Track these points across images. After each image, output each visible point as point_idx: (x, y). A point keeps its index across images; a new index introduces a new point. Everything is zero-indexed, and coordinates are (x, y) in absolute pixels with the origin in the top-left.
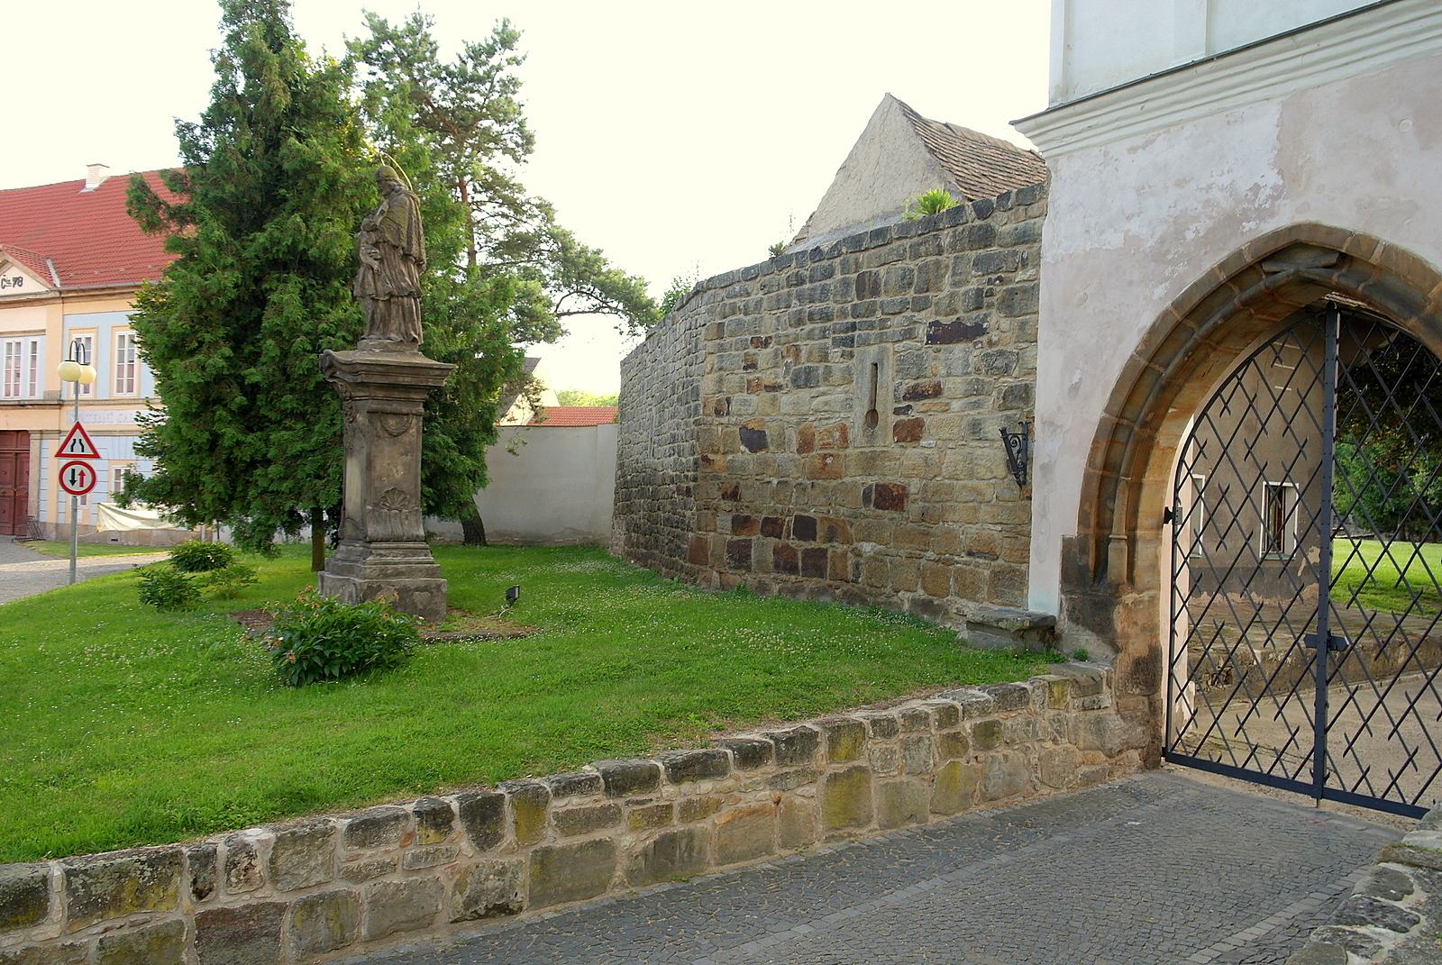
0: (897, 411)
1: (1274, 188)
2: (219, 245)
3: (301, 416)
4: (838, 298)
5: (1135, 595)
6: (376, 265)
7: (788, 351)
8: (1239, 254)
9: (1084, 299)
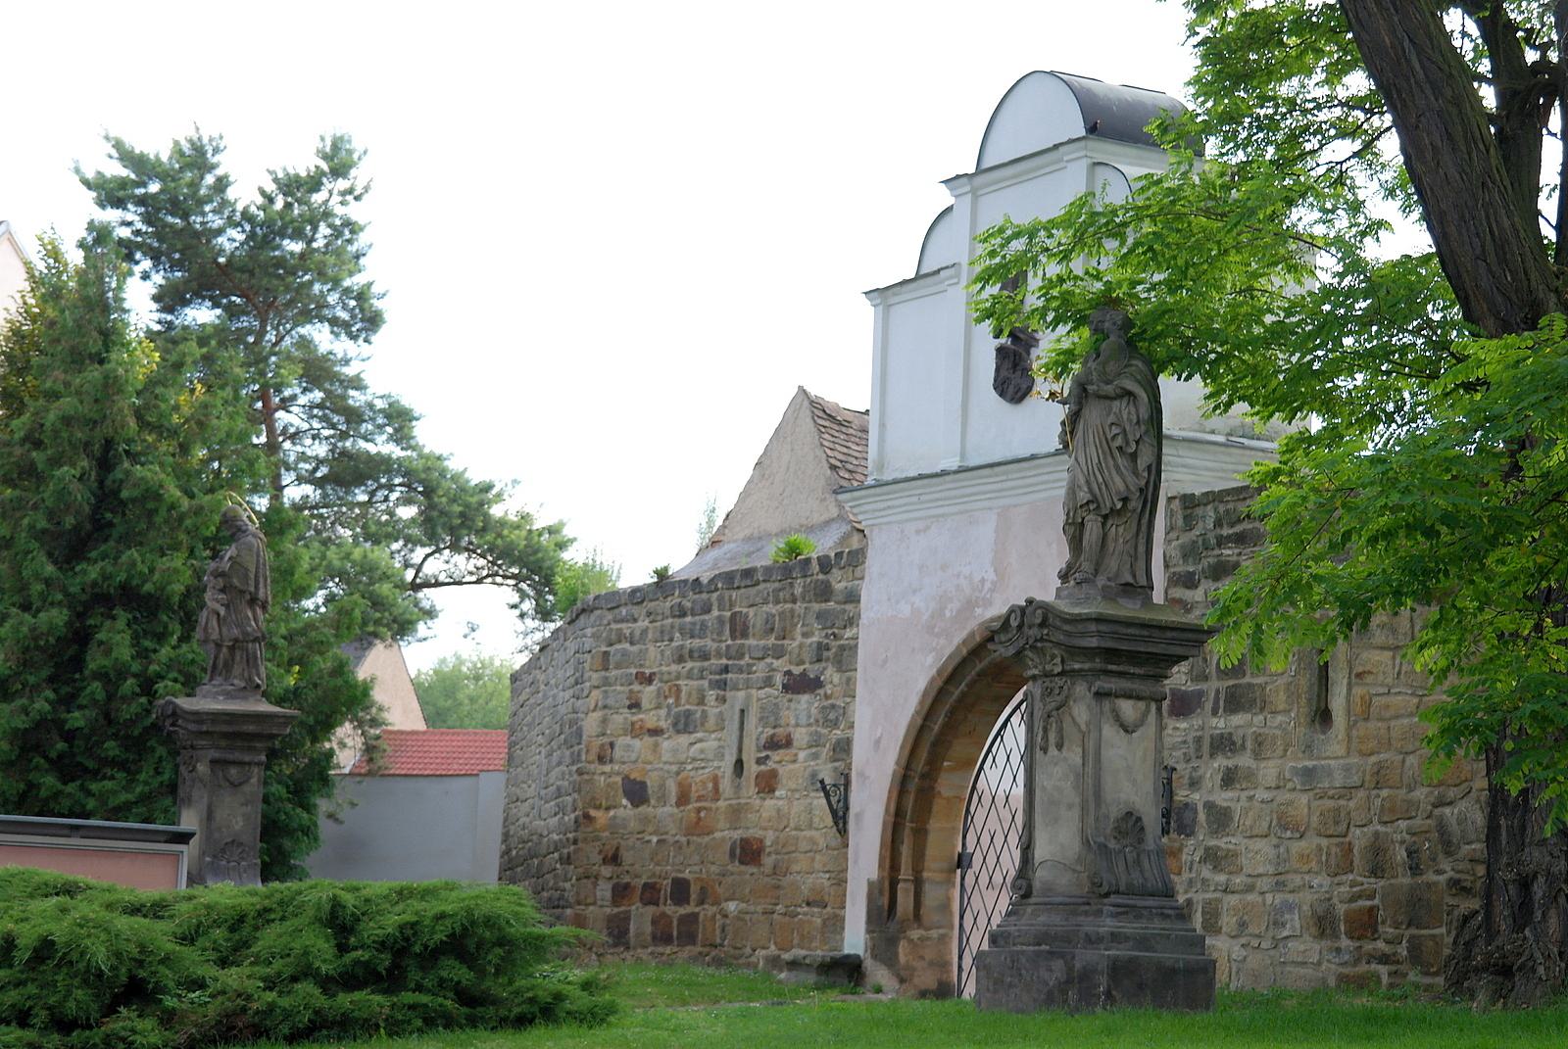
0: (759, 761)
1: (993, 583)
2: (48, 582)
3: (122, 765)
4: (715, 636)
5: (921, 932)
6: (222, 612)
7: (670, 690)
8: (972, 635)
9: (885, 661)
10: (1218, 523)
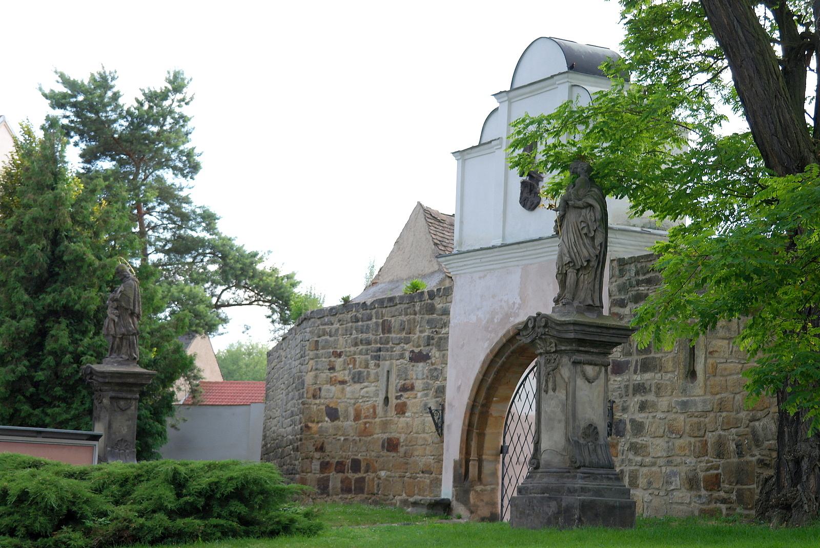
0: (397, 398)
1: (519, 304)
2: (25, 304)
3: (64, 400)
4: (374, 332)
5: (482, 487)
6: (116, 320)
7: (350, 360)
8: (508, 331)
9: (463, 345)
10: (637, 273)
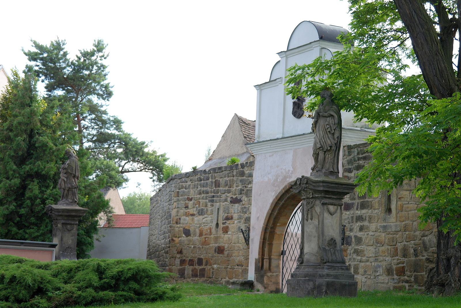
0: (223, 224)
1: (292, 171)
2: (14, 171)
3: (36, 225)
4: (210, 187)
5: (271, 274)
6: (65, 180)
7: (197, 203)
8: (286, 186)
9: (260, 194)
